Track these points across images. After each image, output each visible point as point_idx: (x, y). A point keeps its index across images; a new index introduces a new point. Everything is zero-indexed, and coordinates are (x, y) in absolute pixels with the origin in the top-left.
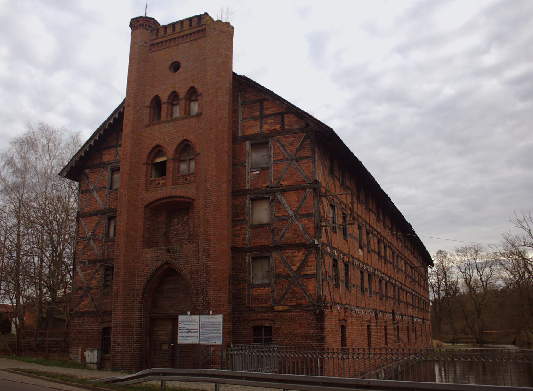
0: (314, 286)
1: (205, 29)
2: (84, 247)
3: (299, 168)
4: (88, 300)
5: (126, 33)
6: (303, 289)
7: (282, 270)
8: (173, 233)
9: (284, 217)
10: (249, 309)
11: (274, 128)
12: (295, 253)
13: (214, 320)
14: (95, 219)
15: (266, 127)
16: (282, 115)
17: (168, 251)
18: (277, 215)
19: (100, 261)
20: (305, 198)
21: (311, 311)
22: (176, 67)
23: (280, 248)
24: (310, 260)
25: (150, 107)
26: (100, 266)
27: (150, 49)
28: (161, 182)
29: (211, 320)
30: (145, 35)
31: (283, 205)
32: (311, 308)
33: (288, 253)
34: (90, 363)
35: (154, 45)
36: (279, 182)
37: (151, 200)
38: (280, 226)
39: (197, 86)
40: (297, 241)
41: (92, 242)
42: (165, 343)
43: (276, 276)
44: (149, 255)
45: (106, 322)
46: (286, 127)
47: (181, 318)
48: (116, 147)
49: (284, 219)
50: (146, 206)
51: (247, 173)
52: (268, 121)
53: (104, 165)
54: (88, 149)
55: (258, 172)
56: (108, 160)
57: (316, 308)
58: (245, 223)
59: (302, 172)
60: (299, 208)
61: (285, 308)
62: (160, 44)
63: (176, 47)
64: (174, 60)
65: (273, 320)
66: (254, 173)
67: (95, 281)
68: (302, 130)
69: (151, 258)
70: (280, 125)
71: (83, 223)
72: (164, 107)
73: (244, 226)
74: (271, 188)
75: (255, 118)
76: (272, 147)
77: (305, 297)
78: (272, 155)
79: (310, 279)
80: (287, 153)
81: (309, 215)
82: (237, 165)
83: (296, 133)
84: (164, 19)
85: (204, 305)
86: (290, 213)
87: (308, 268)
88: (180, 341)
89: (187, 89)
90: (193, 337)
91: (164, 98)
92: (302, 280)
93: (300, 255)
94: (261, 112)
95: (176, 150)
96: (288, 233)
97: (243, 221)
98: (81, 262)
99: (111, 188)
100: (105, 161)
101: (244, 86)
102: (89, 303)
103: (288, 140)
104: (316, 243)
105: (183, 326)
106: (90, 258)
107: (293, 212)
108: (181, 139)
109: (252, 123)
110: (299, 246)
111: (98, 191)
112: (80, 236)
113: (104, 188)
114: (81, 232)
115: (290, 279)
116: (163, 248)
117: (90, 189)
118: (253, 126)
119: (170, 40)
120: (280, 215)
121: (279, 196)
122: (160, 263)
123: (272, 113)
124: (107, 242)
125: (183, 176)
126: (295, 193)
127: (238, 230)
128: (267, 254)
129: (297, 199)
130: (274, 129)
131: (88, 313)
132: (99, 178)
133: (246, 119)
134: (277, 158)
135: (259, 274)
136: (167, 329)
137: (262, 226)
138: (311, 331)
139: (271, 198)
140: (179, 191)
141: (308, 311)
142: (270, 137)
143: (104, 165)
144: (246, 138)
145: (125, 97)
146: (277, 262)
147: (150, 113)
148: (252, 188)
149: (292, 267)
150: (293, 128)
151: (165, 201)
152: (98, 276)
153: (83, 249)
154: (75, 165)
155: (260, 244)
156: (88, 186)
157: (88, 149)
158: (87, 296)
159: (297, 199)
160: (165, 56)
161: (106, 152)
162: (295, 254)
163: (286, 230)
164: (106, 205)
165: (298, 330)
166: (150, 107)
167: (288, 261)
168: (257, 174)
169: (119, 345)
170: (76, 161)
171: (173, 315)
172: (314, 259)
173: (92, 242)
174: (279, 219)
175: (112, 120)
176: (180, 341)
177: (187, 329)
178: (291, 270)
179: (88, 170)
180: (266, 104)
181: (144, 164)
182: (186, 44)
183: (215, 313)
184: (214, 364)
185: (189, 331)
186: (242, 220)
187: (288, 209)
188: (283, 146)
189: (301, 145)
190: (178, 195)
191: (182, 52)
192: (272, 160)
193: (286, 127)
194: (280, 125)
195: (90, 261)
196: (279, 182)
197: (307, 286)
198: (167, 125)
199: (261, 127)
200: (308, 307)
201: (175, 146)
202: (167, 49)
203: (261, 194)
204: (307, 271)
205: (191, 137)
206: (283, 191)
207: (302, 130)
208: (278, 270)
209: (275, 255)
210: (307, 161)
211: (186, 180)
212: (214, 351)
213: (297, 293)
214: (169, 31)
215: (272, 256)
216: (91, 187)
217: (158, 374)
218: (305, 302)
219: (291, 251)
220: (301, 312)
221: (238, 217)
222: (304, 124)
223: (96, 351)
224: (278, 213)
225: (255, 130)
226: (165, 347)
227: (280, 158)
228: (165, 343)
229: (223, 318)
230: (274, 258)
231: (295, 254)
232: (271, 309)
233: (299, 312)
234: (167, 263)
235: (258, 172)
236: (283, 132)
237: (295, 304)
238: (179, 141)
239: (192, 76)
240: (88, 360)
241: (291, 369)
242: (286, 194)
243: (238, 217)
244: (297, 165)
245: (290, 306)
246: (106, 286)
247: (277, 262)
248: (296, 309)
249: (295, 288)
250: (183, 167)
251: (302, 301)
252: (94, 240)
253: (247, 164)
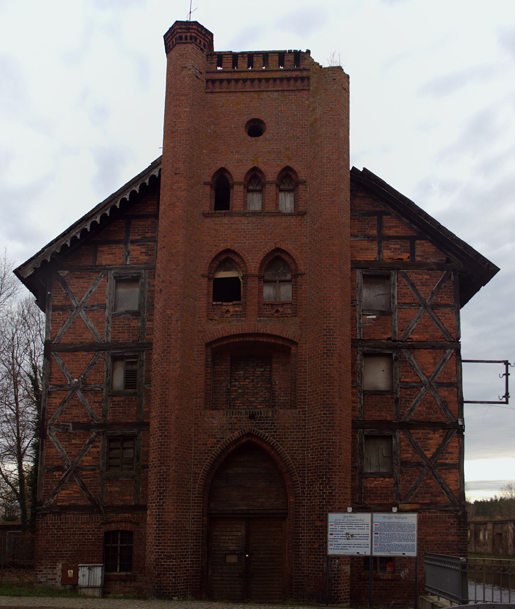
0: (455, 479)
2: (64, 402)
3: (436, 319)
4: (76, 487)
6: (441, 483)
7: (410, 455)
8: (236, 391)
9: (414, 384)
10: (360, 506)
11: (400, 257)
12: (429, 434)
13: (401, 521)
14: (85, 358)
16: (412, 240)
17: (252, 417)
18: (403, 379)
19: (98, 426)
20: (444, 360)
21: (451, 512)
22: (255, 128)
23: (407, 426)
24: (450, 444)
26: (98, 433)
28: (231, 309)
29: (394, 520)
31: (413, 367)
32: (451, 508)
33: (418, 434)
34: (88, 587)
35: (213, 81)
37: (217, 336)
38: (408, 395)
39: (297, 167)
40: (433, 418)
41: (79, 394)
42: (232, 553)
43: (402, 463)
44: (217, 420)
45: (113, 522)
47: (332, 517)
48: (126, 244)
49: (414, 387)
50: (208, 345)
51: (358, 315)
52: (391, 246)
53: (105, 269)
54: (78, 236)
55: (374, 317)
56: (108, 262)
57: (458, 508)
59: (441, 325)
62: (225, 83)
63: (256, 96)
64: (254, 116)
66: (368, 317)
67: (90, 458)
68: (440, 267)
69: (220, 426)
70: (408, 255)
74: (395, 341)
75: (370, 238)
76: (397, 284)
77: (443, 493)
78: (396, 295)
79: (451, 471)
80: (418, 295)
83: (432, 269)
85: (324, 499)
86: (422, 379)
87: (447, 455)
89: (279, 169)
90: (359, 546)
91: (238, 174)
94: (379, 231)
95: (262, 264)
96: (419, 406)
98: (57, 425)
99: (115, 308)
100: (104, 263)
101: (367, 184)
102: (76, 492)
103: (420, 277)
105: (339, 528)
106: (76, 420)
107: (428, 377)
108: (270, 247)
109: (365, 244)
111: (89, 309)
112: (54, 382)
113: (103, 307)
114: (55, 375)
115: (421, 468)
116: (243, 412)
117: (71, 305)
118: (368, 249)
119: (245, 80)
120: (407, 380)
121: (406, 354)
122: (237, 434)
123: (395, 234)
124: (110, 396)
126: (430, 353)
128: (388, 433)
129: (432, 361)
130: (399, 259)
131: (75, 508)
132: (84, 290)
133: (356, 236)
134: (403, 301)
136: (236, 534)
137: (377, 393)
138: (451, 538)
139: (394, 355)
140: (270, 326)
141: (446, 511)
142: (393, 269)
143: (105, 269)
146: (402, 444)
148: (366, 338)
150: (428, 261)
151: (241, 339)
152: (95, 450)
154: (51, 258)
155: (378, 418)
156: (66, 298)
157: (78, 236)
158: (71, 480)
159: (432, 361)
161: (106, 249)
162: (429, 436)
163: (417, 401)
164: (107, 335)
165: (432, 536)
168: (373, 319)
169: (169, 557)
170: (54, 254)
171: (251, 512)
172: (457, 445)
175: (128, 194)
177: (347, 534)
178: (424, 456)
179: (66, 272)
181: (203, 276)
182: (275, 94)
184: (340, 584)
185: (350, 536)
187: (420, 374)
188: (413, 285)
189: (439, 286)
190: (269, 332)
191: (266, 105)
192: (396, 303)
193: (418, 259)
194: (408, 255)
195: (77, 425)
197: (446, 479)
199: (380, 252)
200: (446, 506)
201: (260, 256)
202: (239, 95)
203: (379, 348)
204: (446, 459)
205: (288, 246)
207: (440, 267)
208: (405, 456)
209: (399, 435)
210: (448, 310)
211: (277, 311)
212: (340, 564)
213: (431, 487)
214: (242, 64)
215: (395, 437)
219: (423, 431)
220: (436, 512)
222: (445, 258)
223: (101, 568)
224: (405, 378)
225: (371, 256)
226: (232, 559)
227: (408, 301)
228: (232, 553)
230: (398, 439)
231: (429, 436)
233: (434, 513)
234: (249, 434)
235: (374, 317)
236: (413, 264)
237: (429, 501)
238: (268, 248)
239: (288, 149)
240: (82, 581)
242: (417, 352)
244: (433, 313)
245: (421, 504)
246: (110, 466)
247: (402, 444)
248: (430, 509)
249: (429, 481)
250: (268, 291)
251: (439, 499)
252: (84, 391)
253: (358, 303)
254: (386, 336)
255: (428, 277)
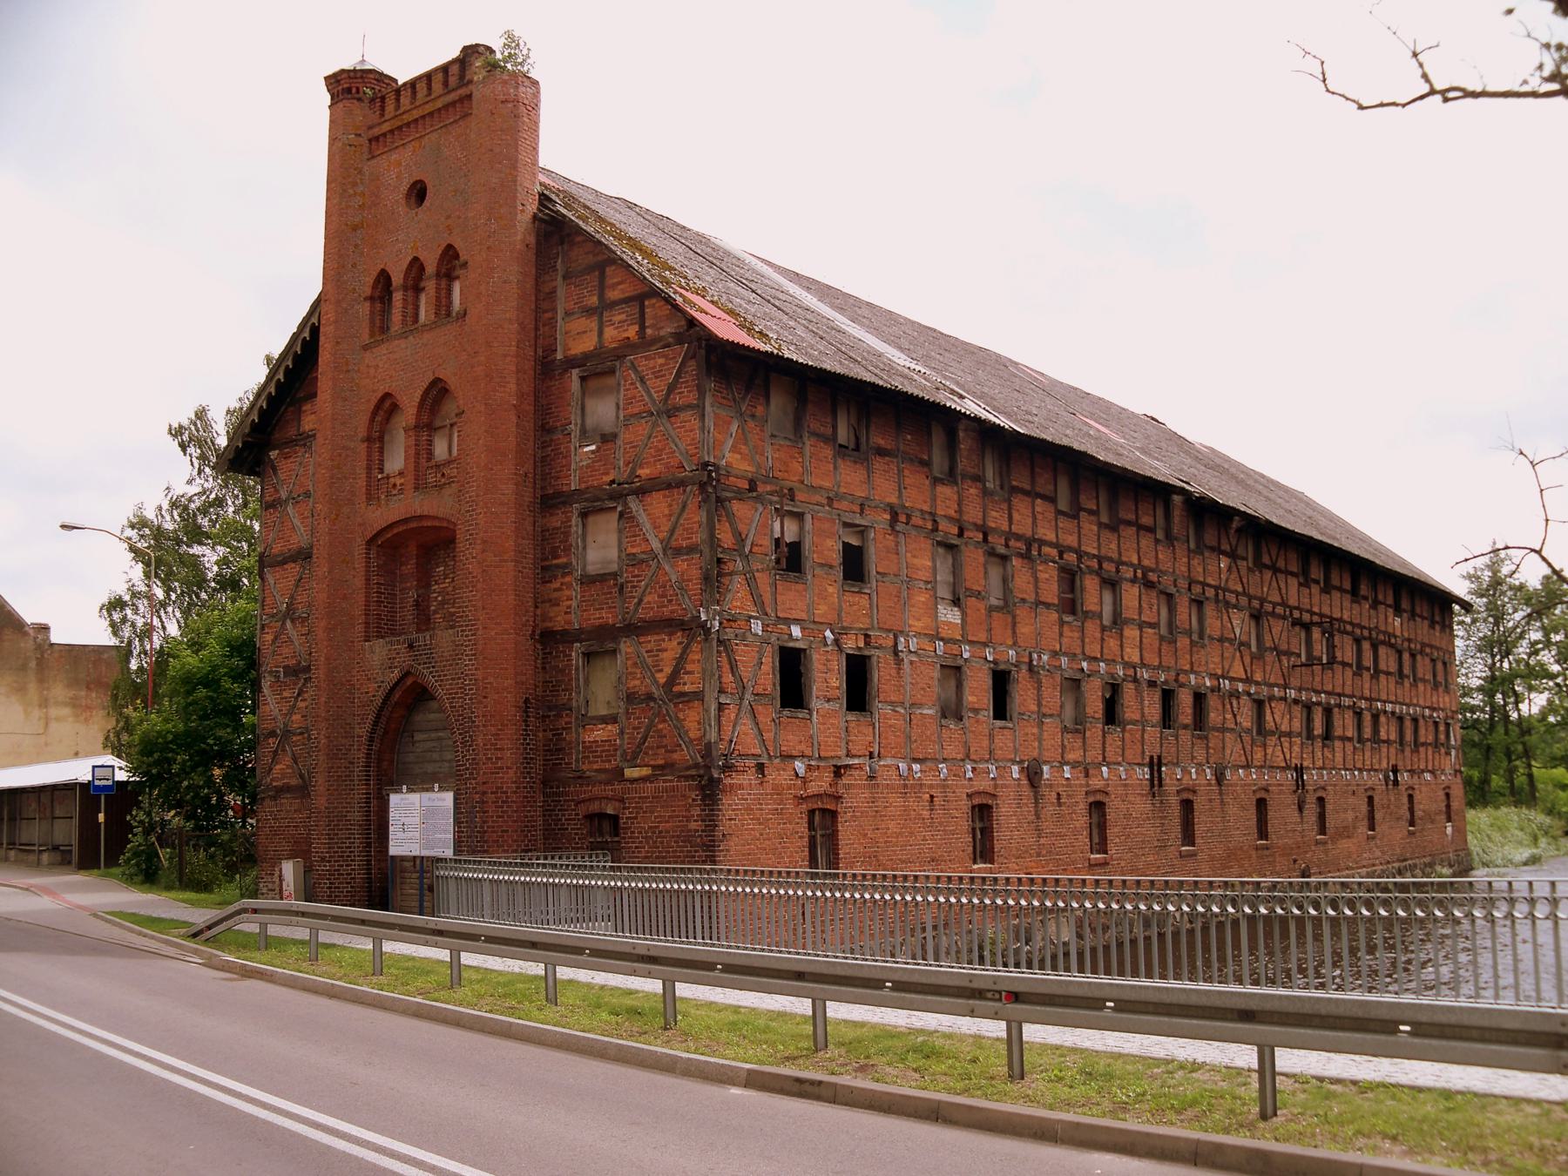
1: (470, 96)
4: (288, 760)
5: (314, 114)
15: (610, 333)
22: (418, 193)
23: (635, 629)
25: (371, 298)
27: (370, 151)
30: (361, 114)
32: (693, 772)
35: (377, 139)
36: (633, 470)
39: (459, 244)
41: (288, 624)
46: (649, 331)
58: (570, 573)
60: (672, 532)
61: (645, 771)
65: (622, 801)
68: (679, 338)
69: (379, 663)
71: (270, 579)
72: (398, 297)
73: (567, 579)
75: (589, 312)
80: (650, 396)
81: (691, 549)
82: (544, 428)
84: (405, 63)
88: (393, 851)
92: (676, 705)
93: (672, 646)
94: (601, 296)
97: (566, 569)
100: (307, 428)
104: (704, 618)
110: (669, 625)
121: (633, 504)
122: (396, 674)
125: (437, 466)
127: (555, 590)
128: (610, 646)
135: (601, 690)
137: (601, 578)
138: (693, 825)
141: (687, 778)
142: (619, 358)
144: (571, 363)
145: (313, 286)
147: (372, 313)
149: (658, 675)
150: (662, 333)
153: (274, 641)
155: (597, 622)
156: (277, 491)
160: (397, 168)
166: (371, 298)
167: (649, 661)
169: (323, 859)
173: (288, 624)
174: (634, 561)
176: (393, 851)
180: (609, 270)
183: (441, 789)
186: (566, 566)
188: (642, 380)
196: (633, 470)
198: (403, 343)
199: (601, 333)
200: (688, 768)
201: (418, 394)
206: (641, 492)
216: (284, 495)
217: (255, 911)
218: (685, 755)
221: (548, 559)
225: (587, 344)
229: (455, 799)
232: (618, 774)
236: (644, 343)
237: (661, 762)
241: (1184, 939)
243: (548, 559)
254: (608, 479)
255: (661, 361)
